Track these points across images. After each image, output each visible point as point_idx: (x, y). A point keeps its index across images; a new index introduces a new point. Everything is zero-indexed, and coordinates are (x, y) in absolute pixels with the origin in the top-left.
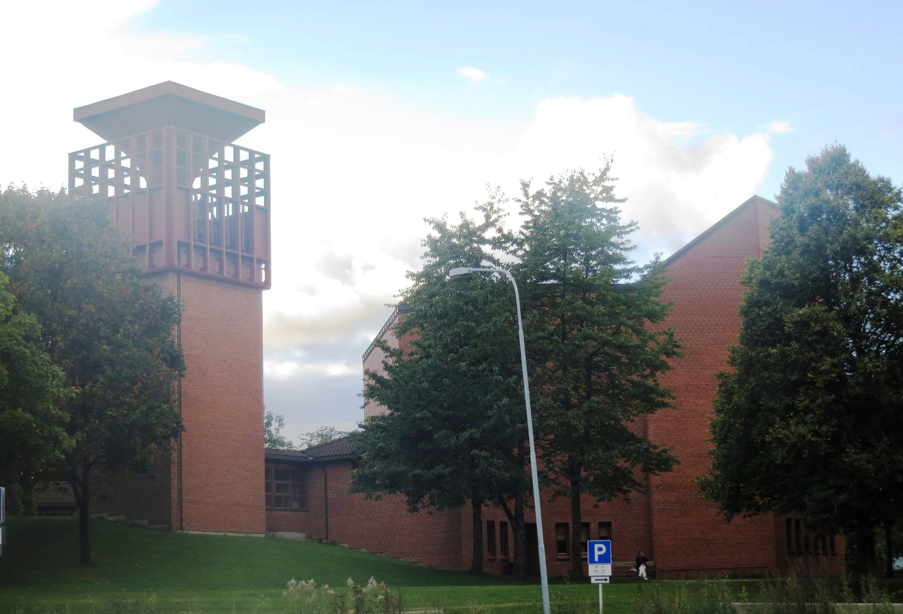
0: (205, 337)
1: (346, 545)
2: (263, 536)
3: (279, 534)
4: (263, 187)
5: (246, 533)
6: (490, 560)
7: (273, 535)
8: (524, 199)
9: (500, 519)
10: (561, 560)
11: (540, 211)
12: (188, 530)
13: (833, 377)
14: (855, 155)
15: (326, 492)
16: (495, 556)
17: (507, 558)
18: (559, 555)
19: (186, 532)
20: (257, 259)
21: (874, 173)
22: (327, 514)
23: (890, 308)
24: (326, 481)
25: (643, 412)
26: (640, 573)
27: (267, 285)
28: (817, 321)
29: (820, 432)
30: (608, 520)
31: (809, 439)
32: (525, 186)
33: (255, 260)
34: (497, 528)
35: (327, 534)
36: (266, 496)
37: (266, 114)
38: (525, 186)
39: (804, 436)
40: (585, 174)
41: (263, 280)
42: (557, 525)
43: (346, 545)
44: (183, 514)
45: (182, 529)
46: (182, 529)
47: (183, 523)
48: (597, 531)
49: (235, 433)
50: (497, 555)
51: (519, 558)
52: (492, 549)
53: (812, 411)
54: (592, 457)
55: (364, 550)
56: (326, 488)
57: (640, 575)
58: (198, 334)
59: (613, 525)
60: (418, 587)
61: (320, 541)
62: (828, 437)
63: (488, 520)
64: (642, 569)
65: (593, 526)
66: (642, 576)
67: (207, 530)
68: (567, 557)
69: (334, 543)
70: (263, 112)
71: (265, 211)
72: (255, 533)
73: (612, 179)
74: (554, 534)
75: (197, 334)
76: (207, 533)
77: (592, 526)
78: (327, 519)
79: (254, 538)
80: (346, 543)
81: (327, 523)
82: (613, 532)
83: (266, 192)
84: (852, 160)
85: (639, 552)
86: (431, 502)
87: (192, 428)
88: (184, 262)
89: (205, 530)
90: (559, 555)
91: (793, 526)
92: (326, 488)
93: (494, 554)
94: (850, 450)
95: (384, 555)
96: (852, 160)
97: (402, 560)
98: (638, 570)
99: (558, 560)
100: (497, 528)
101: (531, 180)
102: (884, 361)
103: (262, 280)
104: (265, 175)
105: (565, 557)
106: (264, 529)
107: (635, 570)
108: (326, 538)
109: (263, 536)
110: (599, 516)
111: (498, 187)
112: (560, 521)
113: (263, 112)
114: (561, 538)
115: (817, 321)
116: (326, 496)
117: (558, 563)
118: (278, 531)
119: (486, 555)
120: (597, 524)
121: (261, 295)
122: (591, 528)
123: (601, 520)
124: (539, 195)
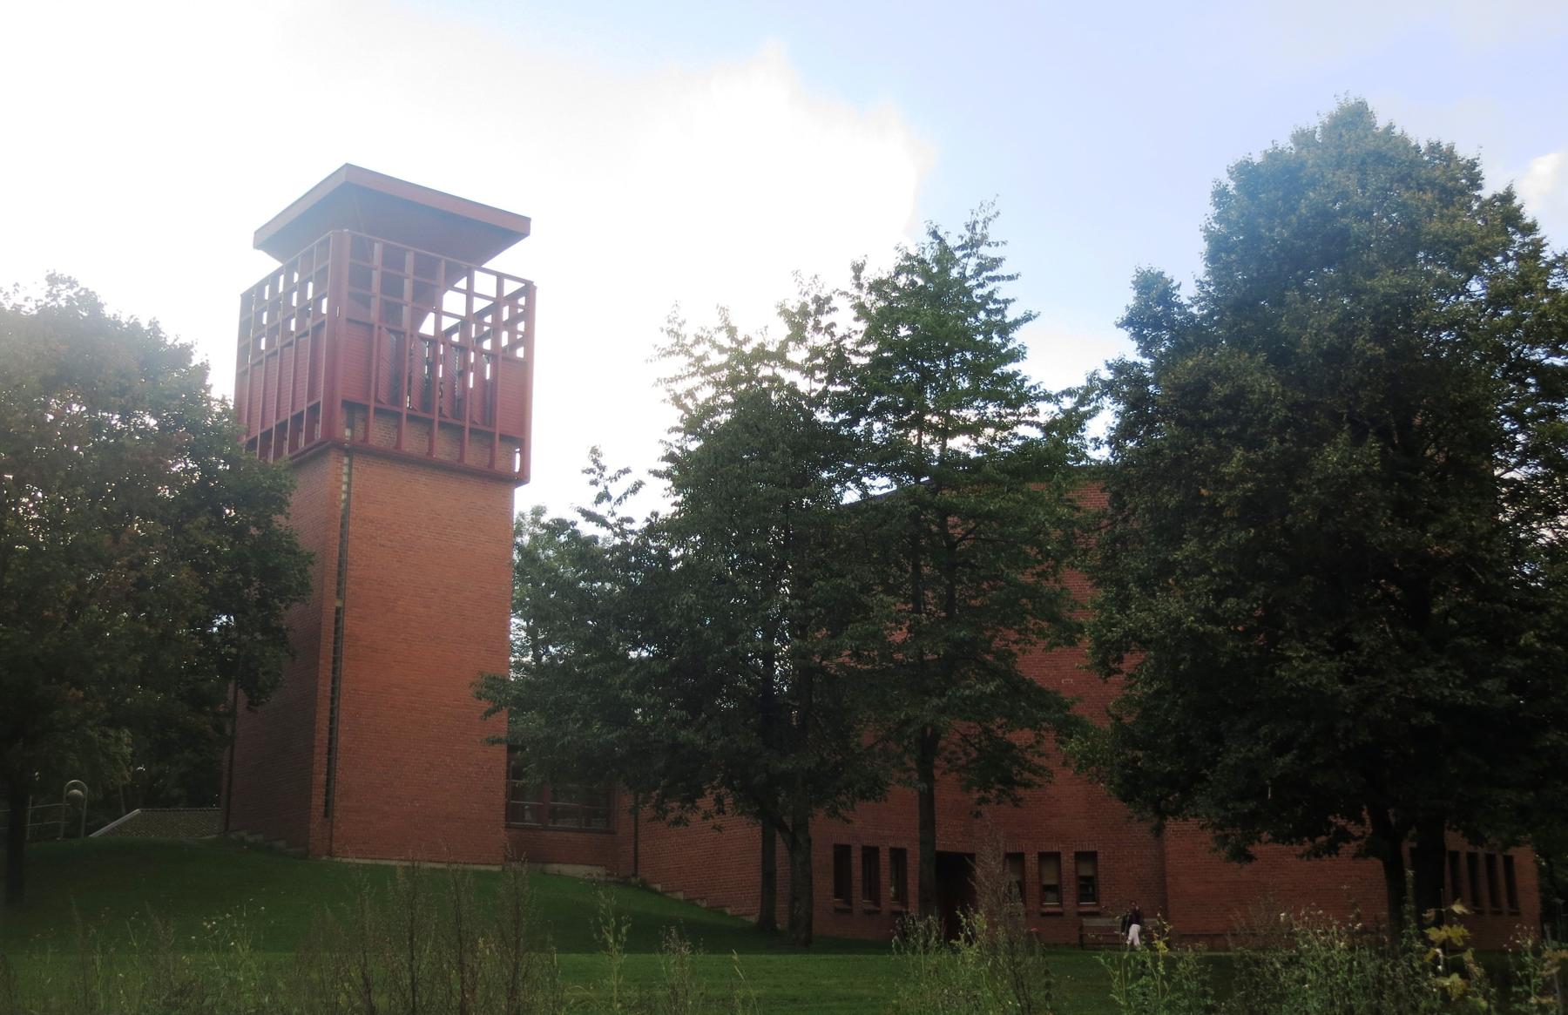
2: (496, 869)
3: (554, 868)
4: (464, 315)
6: (869, 912)
9: (890, 845)
12: (344, 857)
14: (1387, 113)
19: (339, 859)
20: (501, 436)
21: (1420, 132)
25: (1058, 645)
29: (1219, 612)
30: (1092, 849)
32: (858, 269)
34: (885, 858)
35: (636, 868)
36: (507, 804)
38: (858, 269)
44: (334, 830)
45: (330, 854)
46: (330, 854)
47: (334, 845)
48: (1073, 867)
50: (882, 903)
53: (1205, 568)
59: (1100, 857)
62: (1236, 622)
63: (865, 844)
65: (1065, 858)
66: (1132, 943)
70: (527, 220)
72: (482, 864)
76: (383, 862)
77: (1064, 858)
79: (381, 866)
80: (659, 883)
81: (636, 848)
83: (528, 340)
84: (1381, 123)
87: (360, 692)
88: (360, 434)
89: (377, 856)
91: (1482, 868)
94: (1296, 651)
96: (1381, 123)
102: (1373, 452)
104: (528, 315)
108: (635, 875)
109: (496, 869)
110: (1075, 841)
111: (816, 277)
112: (1047, 849)
118: (553, 863)
120: (1073, 854)
121: (513, 493)
122: (1062, 862)
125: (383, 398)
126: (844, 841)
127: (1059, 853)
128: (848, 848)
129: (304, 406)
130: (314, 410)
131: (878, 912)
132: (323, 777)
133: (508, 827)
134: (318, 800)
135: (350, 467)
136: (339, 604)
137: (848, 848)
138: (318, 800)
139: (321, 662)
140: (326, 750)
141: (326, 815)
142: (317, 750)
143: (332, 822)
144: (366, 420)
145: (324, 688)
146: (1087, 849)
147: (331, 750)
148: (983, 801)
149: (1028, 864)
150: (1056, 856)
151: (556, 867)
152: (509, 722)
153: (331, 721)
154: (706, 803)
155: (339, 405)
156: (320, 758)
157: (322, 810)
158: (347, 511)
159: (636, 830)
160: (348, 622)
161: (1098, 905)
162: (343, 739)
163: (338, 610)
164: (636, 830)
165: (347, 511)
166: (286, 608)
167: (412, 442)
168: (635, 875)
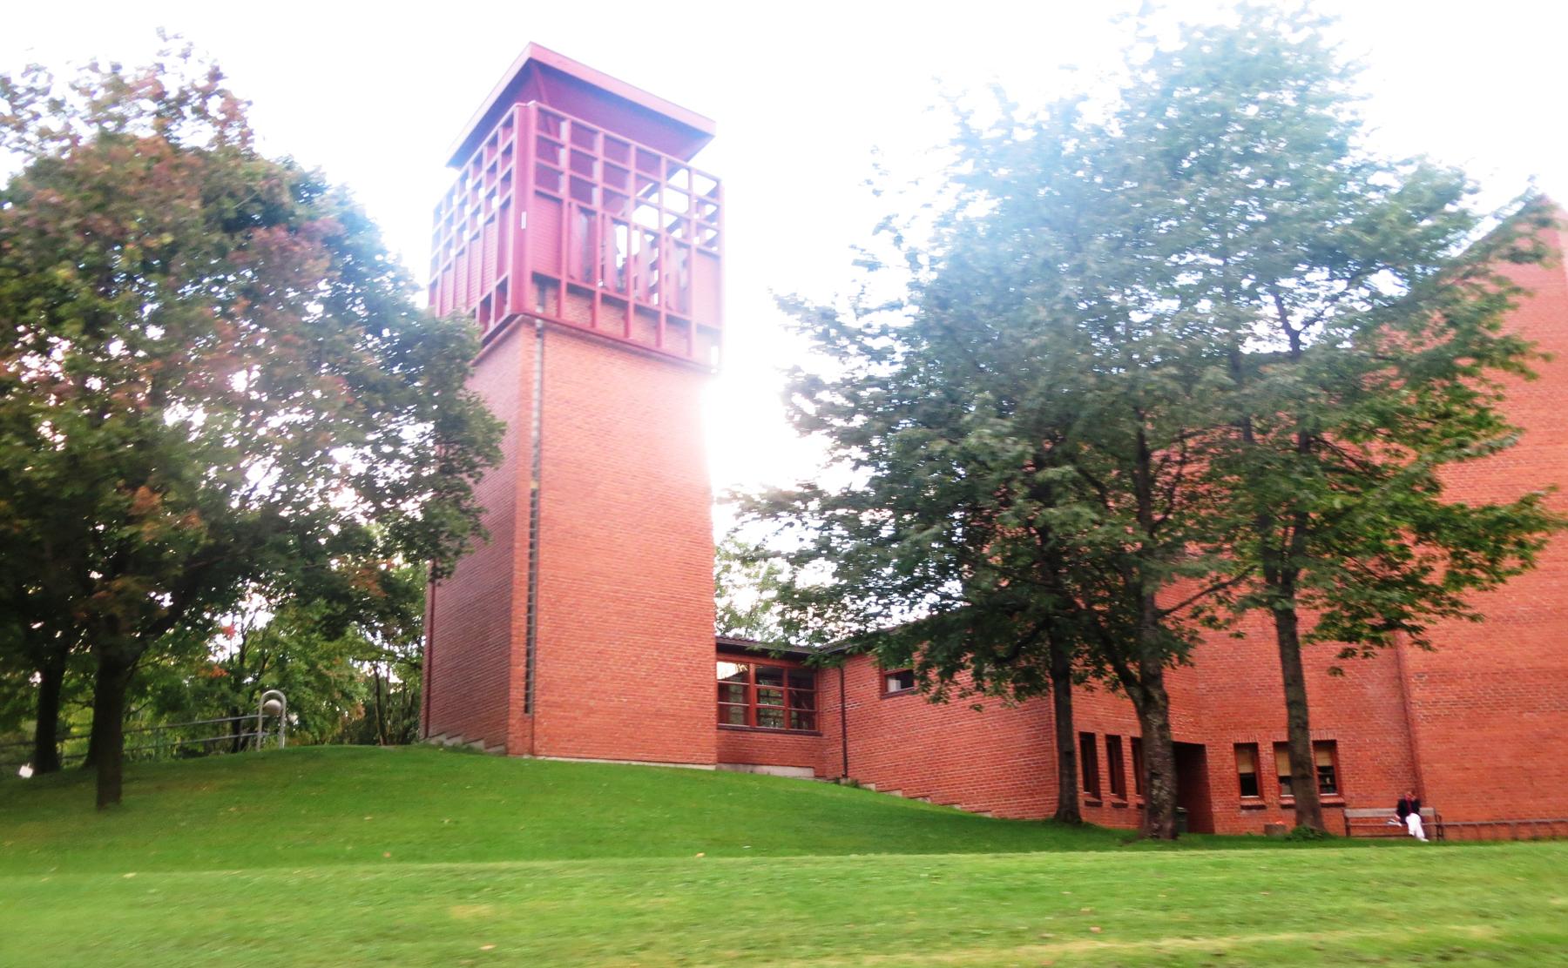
1: (872, 786)
2: (712, 768)
6: (1116, 806)
10: (1249, 808)
11: (1228, 148)
15: (843, 701)
22: (844, 736)
23: (412, 378)
24: (842, 684)
30: (1330, 737)
33: (598, 298)
34: (1127, 748)
42: (1238, 747)
43: (872, 786)
45: (532, 752)
46: (532, 752)
47: (536, 743)
52: (1118, 786)
55: (899, 793)
56: (843, 695)
59: (1340, 746)
61: (837, 781)
63: (1208, 750)
64: (1414, 821)
69: (856, 785)
74: (1233, 763)
78: (845, 744)
82: (1341, 758)
92: (843, 695)
93: (1122, 795)
95: (929, 801)
97: (957, 807)
99: (1243, 807)
100: (1127, 748)
105: (1255, 803)
106: (714, 757)
108: (845, 776)
109: (712, 768)
114: (1246, 769)
116: (843, 708)
117: (1244, 812)
119: (1083, 796)
125: (575, 270)
126: (1089, 730)
127: (1202, 747)
128: (1092, 735)
129: (492, 288)
130: (502, 288)
131: (1125, 806)
132: (522, 669)
133: (719, 728)
134: (519, 648)
135: (543, 354)
136: (534, 485)
137: (1092, 735)
138: (517, 693)
139: (517, 545)
140: (524, 639)
141: (526, 709)
142: (515, 639)
143: (533, 717)
144: (558, 297)
145: (521, 574)
146: (1325, 738)
147: (530, 640)
148: (1345, 654)
149: (1262, 754)
150: (1253, 748)
151: (766, 768)
152: (1046, 264)
153: (530, 609)
154: (964, 677)
155: (528, 278)
156: (519, 648)
157: (522, 703)
158: (539, 444)
159: (844, 730)
160: (545, 505)
161: (1262, 798)
162: (543, 629)
163: (533, 494)
164: (844, 730)
165: (539, 444)
166: (476, 482)
167: (607, 322)
168: (845, 776)
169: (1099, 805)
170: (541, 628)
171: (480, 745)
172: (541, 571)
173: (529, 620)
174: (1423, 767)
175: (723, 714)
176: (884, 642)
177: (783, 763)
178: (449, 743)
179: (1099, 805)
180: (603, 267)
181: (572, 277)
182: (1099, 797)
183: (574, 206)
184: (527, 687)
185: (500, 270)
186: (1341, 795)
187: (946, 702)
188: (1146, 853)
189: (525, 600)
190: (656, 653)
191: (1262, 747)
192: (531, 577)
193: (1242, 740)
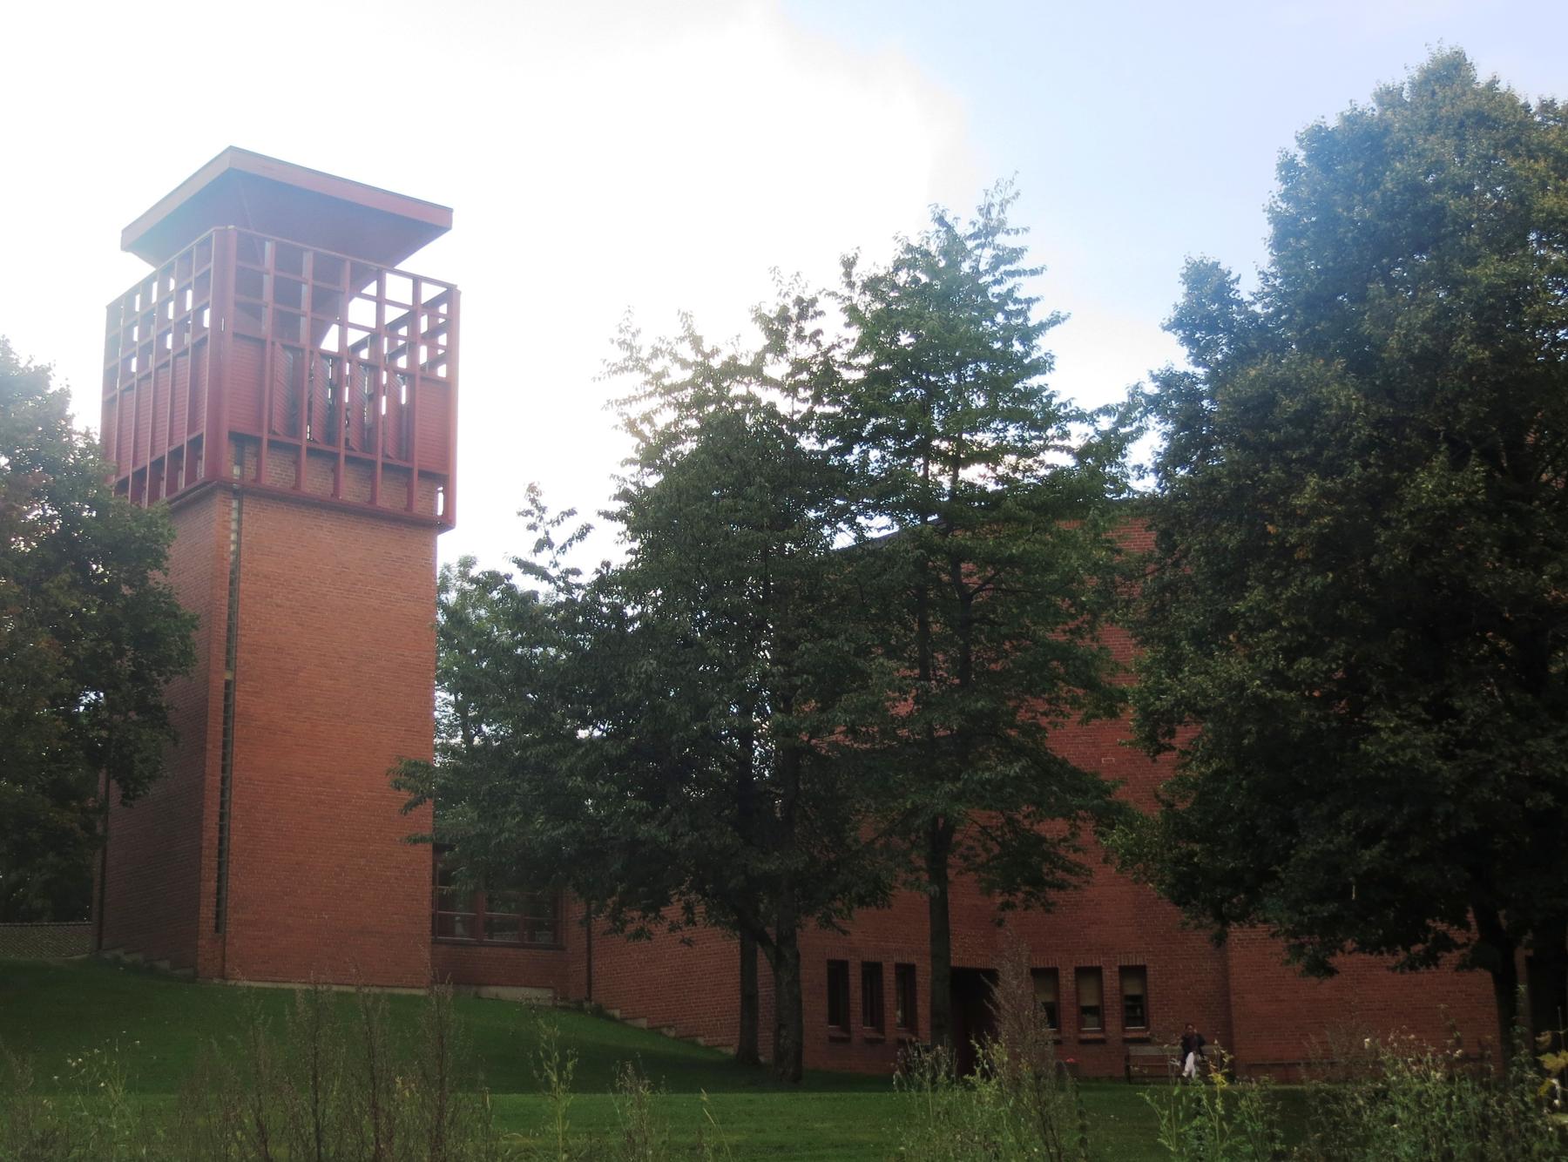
0: (297, 613)
5: (382, 986)
6: (871, 1042)
7: (476, 993)
8: (846, 292)
13: (1326, 526)
16: (883, 1033)
17: (845, 1035)
18: (1129, 1031)
19: (233, 983)
26: (1187, 1069)
27: (446, 523)
28: (1291, 392)
30: (1139, 962)
31: (1255, 695)
37: (454, 214)
38: (849, 264)
39: (1241, 686)
40: (949, 219)
41: (440, 512)
45: (223, 977)
46: (223, 977)
48: (1117, 984)
49: (363, 794)
51: (784, 1033)
54: (913, 803)
57: (1185, 1074)
58: (280, 606)
59: (1150, 972)
60: (691, 1095)
67: (277, 978)
68: (1100, 1036)
70: (447, 212)
71: (445, 392)
73: (1017, 232)
75: (278, 606)
78: (589, 960)
80: (617, 1008)
83: (450, 356)
84: (1482, 77)
85: (1187, 1025)
86: (688, 918)
90: (1129, 1031)
96: (1482, 77)
98: (1184, 1063)
101: (857, 251)
103: (436, 511)
107: (1178, 1064)
108: (589, 999)
109: (421, 992)
113: (447, 212)
114: (1049, 998)
115: (1291, 392)
118: (489, 985)
120: (1117, 969)
123: (1125, 963)
124: (872, 285)
125: (277, 424)
126: (841, 957)
131: (882, 1041)
132: (213, 885)
134: (305, 408)
135: (240, 512)
136: (229, 676)
138: (207, 912)
139: (209, 746)
144: (258, 455)
145: (213, 779)
149: (1063, 981)
150: (1052, 973)
151: (493, 990)
153: (222, 817)
154: (673, 911)
157: (212, 923)
160: (239, 696)
162: (236, 839)
163: (228, 684)
169: (846, 1041)
170: (234, 838)
171: (165, 965)
172: (234, 773)
173: (221, 829)
174: (1233, 998)
175: (441, 926)
176: (574, 886)
177: (514, 982)
178: (127, 959)
179: (846, 1041)
180: (310, 404)
181: (274, 433)
182: (848, 1031)
183: (278, 345)
184: (218, 904)
185: (193, 425)
186: (1103, 1031)
187: (649, 939)
188: (835, 1095)
189: (217, 809)
190: (362, 862)
191: (1062, 973)
192: (223, 781)
193: (1041, 965)
